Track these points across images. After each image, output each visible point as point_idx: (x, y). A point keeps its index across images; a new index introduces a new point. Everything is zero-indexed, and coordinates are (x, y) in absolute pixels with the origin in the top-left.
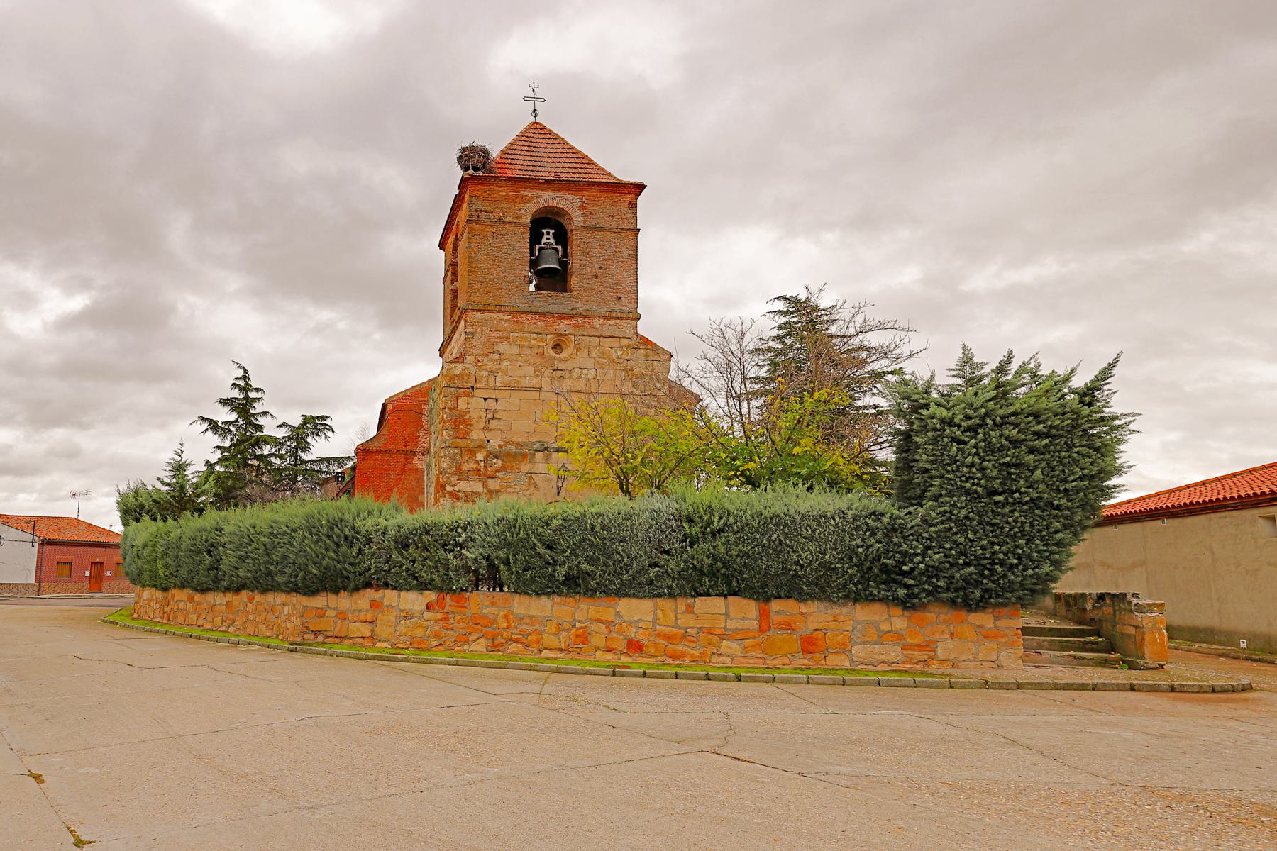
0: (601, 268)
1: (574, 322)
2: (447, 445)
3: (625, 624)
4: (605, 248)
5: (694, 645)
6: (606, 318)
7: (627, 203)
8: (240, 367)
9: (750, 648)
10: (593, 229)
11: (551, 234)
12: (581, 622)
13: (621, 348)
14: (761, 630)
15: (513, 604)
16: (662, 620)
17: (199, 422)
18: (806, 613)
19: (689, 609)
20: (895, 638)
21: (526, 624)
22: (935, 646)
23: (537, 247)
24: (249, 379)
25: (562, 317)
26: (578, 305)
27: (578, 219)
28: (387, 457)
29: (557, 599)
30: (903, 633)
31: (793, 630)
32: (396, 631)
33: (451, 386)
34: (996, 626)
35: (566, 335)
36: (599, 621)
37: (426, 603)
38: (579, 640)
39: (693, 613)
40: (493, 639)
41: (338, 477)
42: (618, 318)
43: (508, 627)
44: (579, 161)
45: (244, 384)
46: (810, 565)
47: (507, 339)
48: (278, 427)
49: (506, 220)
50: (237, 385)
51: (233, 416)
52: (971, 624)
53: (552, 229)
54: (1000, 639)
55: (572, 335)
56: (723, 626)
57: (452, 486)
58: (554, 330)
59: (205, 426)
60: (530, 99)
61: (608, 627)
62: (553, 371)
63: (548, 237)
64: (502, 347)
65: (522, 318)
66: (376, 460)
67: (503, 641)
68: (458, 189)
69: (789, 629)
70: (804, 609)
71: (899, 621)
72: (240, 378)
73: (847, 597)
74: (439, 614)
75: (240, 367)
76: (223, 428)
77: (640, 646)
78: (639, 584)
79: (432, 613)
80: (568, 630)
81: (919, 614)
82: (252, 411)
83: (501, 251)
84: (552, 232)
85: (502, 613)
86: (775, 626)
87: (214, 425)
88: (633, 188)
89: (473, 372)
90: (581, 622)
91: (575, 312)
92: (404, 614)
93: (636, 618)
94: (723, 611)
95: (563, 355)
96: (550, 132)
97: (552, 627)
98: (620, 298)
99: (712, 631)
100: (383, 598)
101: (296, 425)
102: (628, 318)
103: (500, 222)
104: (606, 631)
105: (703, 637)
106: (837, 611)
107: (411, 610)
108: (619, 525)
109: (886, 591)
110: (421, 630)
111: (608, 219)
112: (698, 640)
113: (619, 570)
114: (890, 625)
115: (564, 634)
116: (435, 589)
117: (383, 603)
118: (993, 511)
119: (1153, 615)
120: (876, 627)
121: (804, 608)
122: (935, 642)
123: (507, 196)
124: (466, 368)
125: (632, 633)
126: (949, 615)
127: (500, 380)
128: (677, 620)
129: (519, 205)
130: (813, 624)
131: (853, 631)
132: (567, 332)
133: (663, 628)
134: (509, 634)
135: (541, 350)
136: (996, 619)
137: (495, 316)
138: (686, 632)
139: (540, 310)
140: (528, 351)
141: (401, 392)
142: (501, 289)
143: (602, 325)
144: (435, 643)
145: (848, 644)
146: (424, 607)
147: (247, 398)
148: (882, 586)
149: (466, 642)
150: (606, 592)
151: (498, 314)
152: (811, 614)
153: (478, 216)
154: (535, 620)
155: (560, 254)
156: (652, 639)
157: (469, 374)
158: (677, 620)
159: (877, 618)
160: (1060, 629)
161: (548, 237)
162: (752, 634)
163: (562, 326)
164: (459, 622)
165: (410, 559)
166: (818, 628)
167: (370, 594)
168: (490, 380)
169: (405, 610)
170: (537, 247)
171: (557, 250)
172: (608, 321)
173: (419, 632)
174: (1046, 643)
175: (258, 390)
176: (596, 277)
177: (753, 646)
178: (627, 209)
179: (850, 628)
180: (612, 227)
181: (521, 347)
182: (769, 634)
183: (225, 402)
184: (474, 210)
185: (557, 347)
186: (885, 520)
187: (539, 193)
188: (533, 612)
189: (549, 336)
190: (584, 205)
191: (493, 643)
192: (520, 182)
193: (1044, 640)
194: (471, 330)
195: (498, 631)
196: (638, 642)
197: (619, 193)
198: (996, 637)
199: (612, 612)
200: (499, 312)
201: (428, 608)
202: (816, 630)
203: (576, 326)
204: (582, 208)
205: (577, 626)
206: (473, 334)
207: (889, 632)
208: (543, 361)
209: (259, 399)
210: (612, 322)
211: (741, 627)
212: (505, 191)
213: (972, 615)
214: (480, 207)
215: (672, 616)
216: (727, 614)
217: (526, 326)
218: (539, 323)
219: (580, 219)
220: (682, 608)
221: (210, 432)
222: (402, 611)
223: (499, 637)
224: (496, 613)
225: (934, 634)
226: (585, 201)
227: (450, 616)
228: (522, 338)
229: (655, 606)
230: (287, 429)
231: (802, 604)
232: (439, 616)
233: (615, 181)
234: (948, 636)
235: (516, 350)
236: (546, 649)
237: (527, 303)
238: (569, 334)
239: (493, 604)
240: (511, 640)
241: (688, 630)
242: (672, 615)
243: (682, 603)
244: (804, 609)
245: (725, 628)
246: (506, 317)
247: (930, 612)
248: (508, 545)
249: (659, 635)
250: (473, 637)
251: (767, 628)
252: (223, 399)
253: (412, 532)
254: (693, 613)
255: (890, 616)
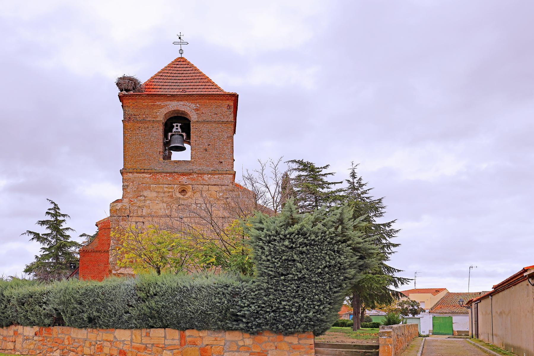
0: (209, 145)
1: (192, 177)
2: (113, 248)
3: (118, 342)
4: (212, 133)
5: (150, 352)
6: (211, 174)
7: (227, 106)
8: (52, 203)
9: (176, 354)
10: (204, 122)
11: (179, 126)
12: (99, 341)
13: (222, 191)
14: (181, 345)
15: (71, 332)
16: (134, 340)
17: (27, 234)
18: (202, 336)
19: (148, 335)
20: (246, 349)
21: (77, 342)
22: (267, 353)
23: (170, 134)
24: (58, 209)
25: (183, 174)
26: (194, 167)
27: (193, 117)
28: (98, 254)
29: (89, 330)
30: (250, 346)
31: (196, 345)
32: (22, 346)
33: (115, 215)
34: (299, 343)
35: (187, 185)
36: (107, 341)
37: (34, 332)
38: (99, 350)
39: (149, 336)
40: (63, 350)
41: (71, 266)
42: (220, 174)
43: (69, 344)
44: (203, 81)
45: (55, 212)
46: (197, 312)
47: (149, 188)
48: (80, 236)
49: (147, 120)
50: (51, 213)
51: (49, 231)
52: (286, 342)
53: (179, 123)
54: (301, 350)
55: (190, 184)
56: (163, 343)
57: (116, 271)
58: (179, 182)
59: (32, 236)
60: (178, 43)
61: (111, 344)
62: (179, 205)
63: (177, 128)
64: (145, 193)
65: (158, 176)
66: (92, 256)
67: (67, 351)
68: (121, 102)
69: (194, 345)
70: (201, 335)
71: (248, 340)
72: (52, 209)
73: (219, 328)
74: (40, 338)
75: (52, 203)
76: (43, 238)
77: (125, 353)
78: (122, 322)
79: (37, 337)
80: (94, 345)
81: (259, 337)
82: (61, 228)
83: (144, 138)
84: (179, 125)
85: (66, 337)
86: (188, 343)
87: (37, 236)
88: (230, 97)
89: (128, 207)
90: (99, 341)
91: (191, 171)
92: (25, 338)
93: (123, 339)
94: (163, 336)
95: (186, 196)
96: (189, 63)
97: (87, 344)
98: (221, 162)
99: (158, 345)
100: (18, 329)
101: (92, 235)
102: (226, 174)
103: (144, 121)
104: (110, 346)
105: (154, 349)
106: (217, 335)
107: (28, 336)
108: (110, 292)
109: (237, 325)
110: (33, 345)
111: (214, 116)
112: (152, 350)
113: (111, 315)
114: (244, 343)
115: (92, 347)
116: (37, 325)
117: (18, 332)
118: (283, 284)
119: (385, 337)
120: (236, 344)
121: (201, 334)
122: (267, 351)
123: (147, 106)
124: (124, 206)
125: (121, 346)
126: (274, 338)
127: (145, 212)
128: (142, 340)
129: (155, 111)
130: (205, 342)
131: (225, 345)
132: (187, 183)
133: (135, 344)
134: (69, 347)
135: (170, 194)
136: (299, 339)
137: (141, 175)
138: (147, 346)
139: (169, 171)
140: (162, 195)
141: (106, 218)
142: (145, 160)
143: (210, 178)
144: (38, 352)
145: (222, 352)
146: (34, 334)
147: (57, 220)
148: (234, 323)
149: (52, 352)
150: (108, 326)
151: (142, 174)
152: (205, 337)
153: (130, 118)
154: (80, 340)
155: (184, 137)
156: (130, 349)
157: (126, 209)
158: (142, 340)
159: (237, 339)
160: (360, 345)
161: (177, 128)
162: (176, 347)
163: (184, 179)
164: (49, 341)
165: (25, 310)
166: (208, 344)
167: (13, 328)
168: (139, 212)
169: (26, 335)
170: (170, 134)
171: (182, 136)
172: (214, 176)
173: (32, 347)
174: (344, 352)
175: (64, 215)
176: (206, 150)
177: (177, 353)
178: (226, 109)
179: (223, 344)
180: (216, 120)
181: (158, 192)
182: (185, 347)
183: (43, 223)
184: (126, 114)
185: (183, 191)
186: (230, 289)
187: (169, 103)
188: (80, 336)
189: (176, 186)
190: (198, 108)
191: (63, 352)
192: (155, 97)
193: (343, 351)
194: (127, 184)
195: (64, 346)
196: (124, 351)
197: (220, 100)
198: (299, 348)
199: (112, 336)
200: (143, 173)
201: (36, 334)
202: (207, 345)
203: (193, 179)
204: (197, 110)
205: (98, 343)
206: (127, 186)
207: (243, 346)
208: (172, 200)
209: (64, 221)
210: (216, 176)
211: (171, 344)
212: (148, 102)
213: (286, 337)
214: (131, 112)
215: (139, 338)
216: (165, 337)
217: (161, 180)
218: (169, 179)
219: (196, 116)
220: (144, 334)
221: (35, 240)
222: (25, 336)
223: (65, 349)
224: (64, 337)
225: (266, 347)
226: (199, 106)
227: (45, 338)
228: (159, 187)
229: (132, 333)
230: (86, 237)
231: (200, 332)
232: (41, 339)
233: (218, 93)
234: (274, 348)
235: (155, 194)
236: (85, 355)
237: (162, 167)
238: (188, 184)
239: (62, 333)
240: (70, 350)
241: (147, 345)
242: (139, 338)
243: (144, 332)
244: (201, 335)
245: (164, 344)
246: (148, 176)
247: (264, 336)
248: (63, 303)
249: (133, 348)
250: (55, 349)
251: (184, 344)
252: (41, 221)
253: (24, 297)
254: (149, 336)
255: (244, 338)
